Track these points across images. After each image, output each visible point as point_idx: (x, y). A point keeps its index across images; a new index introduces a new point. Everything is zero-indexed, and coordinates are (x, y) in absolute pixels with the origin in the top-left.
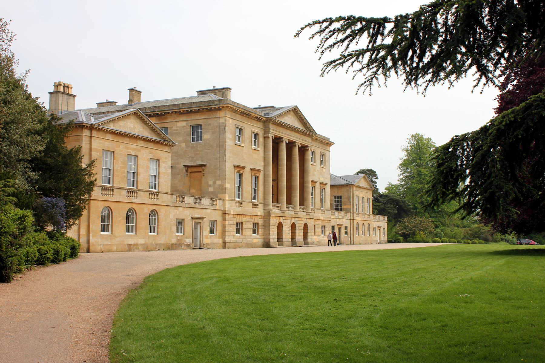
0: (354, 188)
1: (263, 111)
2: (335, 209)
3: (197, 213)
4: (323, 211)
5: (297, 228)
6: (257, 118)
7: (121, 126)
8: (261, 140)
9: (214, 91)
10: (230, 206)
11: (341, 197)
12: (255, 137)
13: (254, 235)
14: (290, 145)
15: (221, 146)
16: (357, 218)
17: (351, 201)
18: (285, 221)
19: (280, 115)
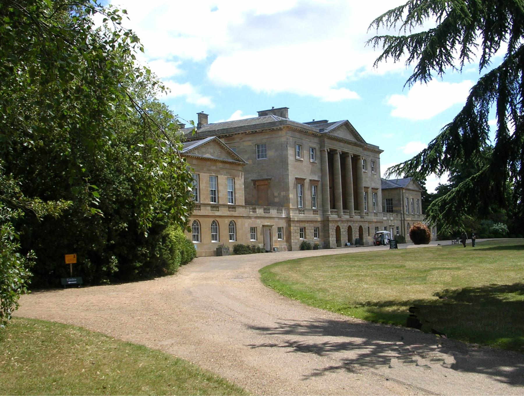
0: (404, 191)
1: (317, 127)
2: (387, 212)
3: (267, 223)
4: (376, 214)
5: (353, 230)
6: (313, 134)
7: (203, 152)
8: (318, 153)
9: (273, 111)
10: (294, 215)
11: (392, 199)
12: (313, 151)
13: (315, 238)
14: (344, 156)
15: (284, 162)
16: (407, 219)
17: (402, 203)
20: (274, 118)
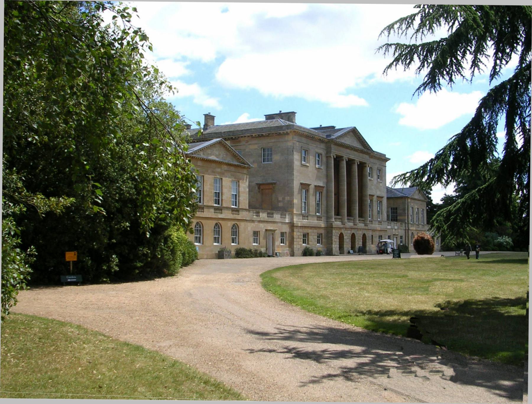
3: (270, 227)
8: (324, 159)
9: (281, 115)
12: (319, 157)
14: (350, 163)
15: (290, 167)
18: (346, 232)
19: (341, 136)
20: (282, 122)
